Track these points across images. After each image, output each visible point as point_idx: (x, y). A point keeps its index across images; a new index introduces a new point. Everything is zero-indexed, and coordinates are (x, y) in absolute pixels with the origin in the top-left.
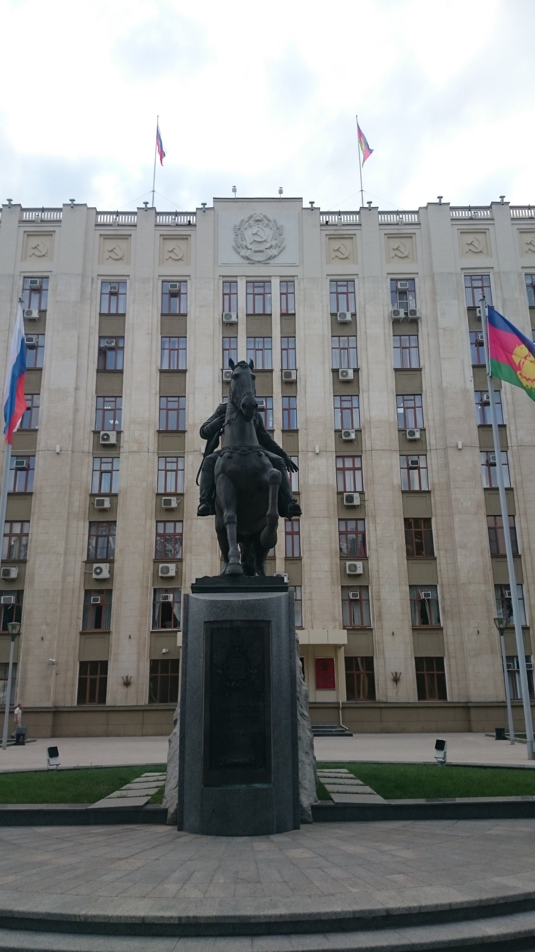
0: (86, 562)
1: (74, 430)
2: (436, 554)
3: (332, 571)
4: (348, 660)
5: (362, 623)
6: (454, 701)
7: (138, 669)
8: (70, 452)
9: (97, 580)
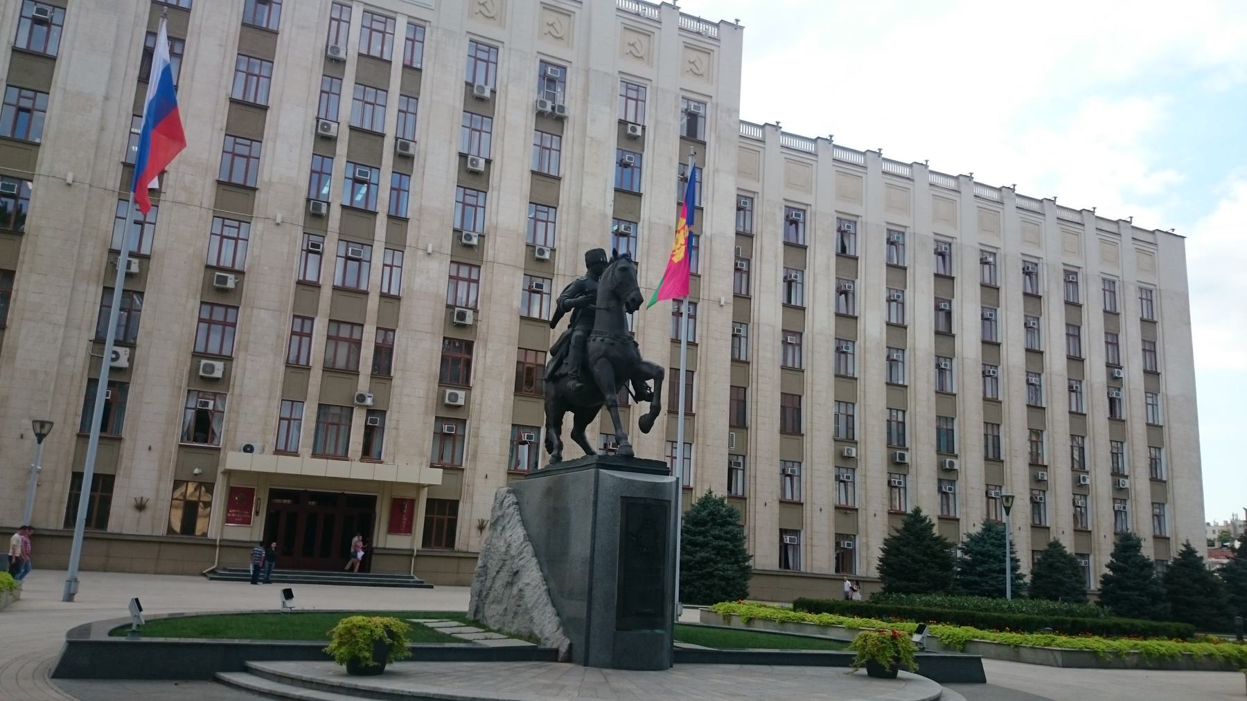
3: (427, 398)
4: (430, 502)
5: (452, 461)
7: (158, 490)
8: (87, 186)
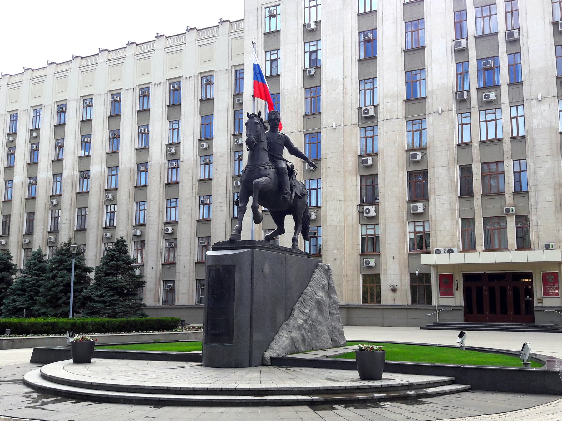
0: (360, 205)
1: (344, 109)
3: (556, 201)
7: (401, 280)
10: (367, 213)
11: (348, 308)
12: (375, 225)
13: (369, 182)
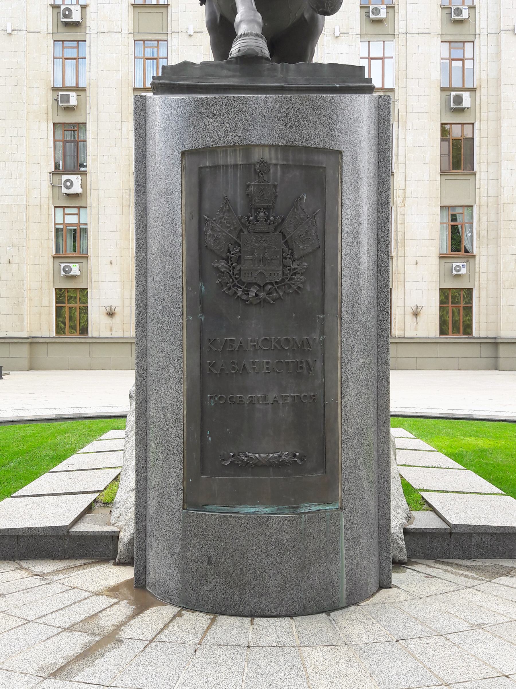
0: (53, 173)
2: (476, 168)
6: (481, 336)
9: (67, 195)
10: (67, 187)
11: (31, 343)
12: (79, 208)
13: (69, 136)
